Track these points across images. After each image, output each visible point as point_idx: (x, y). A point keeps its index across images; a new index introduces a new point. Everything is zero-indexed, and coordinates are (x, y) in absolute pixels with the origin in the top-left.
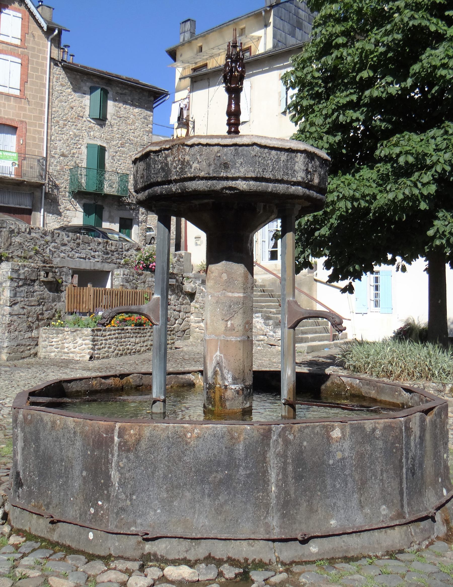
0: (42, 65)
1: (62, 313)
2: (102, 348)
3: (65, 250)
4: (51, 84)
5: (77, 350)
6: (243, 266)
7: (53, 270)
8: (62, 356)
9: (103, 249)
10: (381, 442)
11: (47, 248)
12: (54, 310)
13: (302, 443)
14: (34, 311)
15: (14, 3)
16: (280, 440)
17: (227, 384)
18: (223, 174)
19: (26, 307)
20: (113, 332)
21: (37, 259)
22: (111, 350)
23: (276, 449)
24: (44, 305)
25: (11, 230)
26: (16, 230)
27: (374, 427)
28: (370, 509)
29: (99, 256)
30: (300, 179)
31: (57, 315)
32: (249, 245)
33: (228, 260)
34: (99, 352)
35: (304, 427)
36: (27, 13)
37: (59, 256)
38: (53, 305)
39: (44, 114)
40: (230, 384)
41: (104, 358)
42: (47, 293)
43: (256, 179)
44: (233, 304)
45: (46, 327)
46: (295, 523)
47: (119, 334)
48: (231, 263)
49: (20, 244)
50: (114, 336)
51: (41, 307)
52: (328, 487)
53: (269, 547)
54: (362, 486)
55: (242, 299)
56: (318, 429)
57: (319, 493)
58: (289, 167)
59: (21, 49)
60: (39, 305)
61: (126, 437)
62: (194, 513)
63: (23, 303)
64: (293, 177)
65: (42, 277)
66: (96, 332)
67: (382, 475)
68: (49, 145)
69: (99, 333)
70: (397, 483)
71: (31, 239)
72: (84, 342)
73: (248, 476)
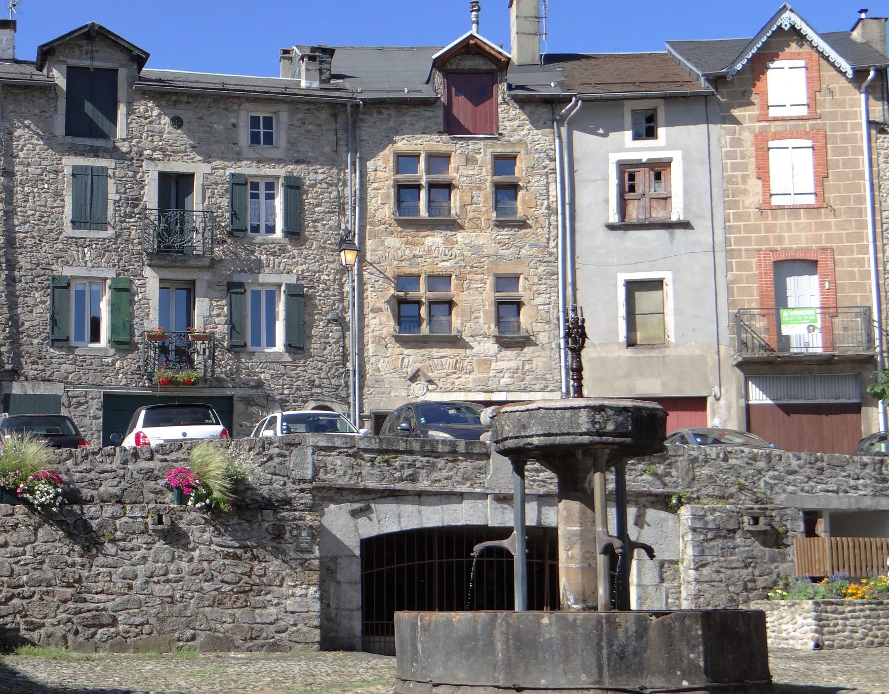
0: (854, 139)
1: (790, 580)
2: (839, 631)
3: (794, 480)
4: (875, 169)
5: (797, 634)
7: (768, 513)
8: (779, 644)
9: (873, 474)
11: (759, 479)
12: (774, 576)
14: (737, 576)
15: (789, 46)
18: (523, 434)
19: (722, 570)
20: (858, 608)
21: (743, 497)
22: (856, 635)
24: (755, 567)
25: (691, 457)
26: (701, 458)
29: (866, 486)
30: (584, 430)
31: (781, 583)
32: (586, 485)
33: (567, 498)
34: (831, 637)
36: (816, 55)
37: (784, 491)
38: (772, 567)
39: (866, 227)
41: (843, 647)
42: (758, 548)
43: (545, 435)
45: (759, 601)
47: (872, 610)
49: (710, 477)
50: (862, 614)
51: (750, 570)
54: (567, 658)
56: (531, 617)
58: (573, 422)
59: (811, 122)
60: (746, 567)
63: (716, 564)
65: (746, 525)
66: (822, 606)
68: (881, 282)
69: (829, 608)
71: (730, 469)
72: (805, 622)
73: (484, 646)
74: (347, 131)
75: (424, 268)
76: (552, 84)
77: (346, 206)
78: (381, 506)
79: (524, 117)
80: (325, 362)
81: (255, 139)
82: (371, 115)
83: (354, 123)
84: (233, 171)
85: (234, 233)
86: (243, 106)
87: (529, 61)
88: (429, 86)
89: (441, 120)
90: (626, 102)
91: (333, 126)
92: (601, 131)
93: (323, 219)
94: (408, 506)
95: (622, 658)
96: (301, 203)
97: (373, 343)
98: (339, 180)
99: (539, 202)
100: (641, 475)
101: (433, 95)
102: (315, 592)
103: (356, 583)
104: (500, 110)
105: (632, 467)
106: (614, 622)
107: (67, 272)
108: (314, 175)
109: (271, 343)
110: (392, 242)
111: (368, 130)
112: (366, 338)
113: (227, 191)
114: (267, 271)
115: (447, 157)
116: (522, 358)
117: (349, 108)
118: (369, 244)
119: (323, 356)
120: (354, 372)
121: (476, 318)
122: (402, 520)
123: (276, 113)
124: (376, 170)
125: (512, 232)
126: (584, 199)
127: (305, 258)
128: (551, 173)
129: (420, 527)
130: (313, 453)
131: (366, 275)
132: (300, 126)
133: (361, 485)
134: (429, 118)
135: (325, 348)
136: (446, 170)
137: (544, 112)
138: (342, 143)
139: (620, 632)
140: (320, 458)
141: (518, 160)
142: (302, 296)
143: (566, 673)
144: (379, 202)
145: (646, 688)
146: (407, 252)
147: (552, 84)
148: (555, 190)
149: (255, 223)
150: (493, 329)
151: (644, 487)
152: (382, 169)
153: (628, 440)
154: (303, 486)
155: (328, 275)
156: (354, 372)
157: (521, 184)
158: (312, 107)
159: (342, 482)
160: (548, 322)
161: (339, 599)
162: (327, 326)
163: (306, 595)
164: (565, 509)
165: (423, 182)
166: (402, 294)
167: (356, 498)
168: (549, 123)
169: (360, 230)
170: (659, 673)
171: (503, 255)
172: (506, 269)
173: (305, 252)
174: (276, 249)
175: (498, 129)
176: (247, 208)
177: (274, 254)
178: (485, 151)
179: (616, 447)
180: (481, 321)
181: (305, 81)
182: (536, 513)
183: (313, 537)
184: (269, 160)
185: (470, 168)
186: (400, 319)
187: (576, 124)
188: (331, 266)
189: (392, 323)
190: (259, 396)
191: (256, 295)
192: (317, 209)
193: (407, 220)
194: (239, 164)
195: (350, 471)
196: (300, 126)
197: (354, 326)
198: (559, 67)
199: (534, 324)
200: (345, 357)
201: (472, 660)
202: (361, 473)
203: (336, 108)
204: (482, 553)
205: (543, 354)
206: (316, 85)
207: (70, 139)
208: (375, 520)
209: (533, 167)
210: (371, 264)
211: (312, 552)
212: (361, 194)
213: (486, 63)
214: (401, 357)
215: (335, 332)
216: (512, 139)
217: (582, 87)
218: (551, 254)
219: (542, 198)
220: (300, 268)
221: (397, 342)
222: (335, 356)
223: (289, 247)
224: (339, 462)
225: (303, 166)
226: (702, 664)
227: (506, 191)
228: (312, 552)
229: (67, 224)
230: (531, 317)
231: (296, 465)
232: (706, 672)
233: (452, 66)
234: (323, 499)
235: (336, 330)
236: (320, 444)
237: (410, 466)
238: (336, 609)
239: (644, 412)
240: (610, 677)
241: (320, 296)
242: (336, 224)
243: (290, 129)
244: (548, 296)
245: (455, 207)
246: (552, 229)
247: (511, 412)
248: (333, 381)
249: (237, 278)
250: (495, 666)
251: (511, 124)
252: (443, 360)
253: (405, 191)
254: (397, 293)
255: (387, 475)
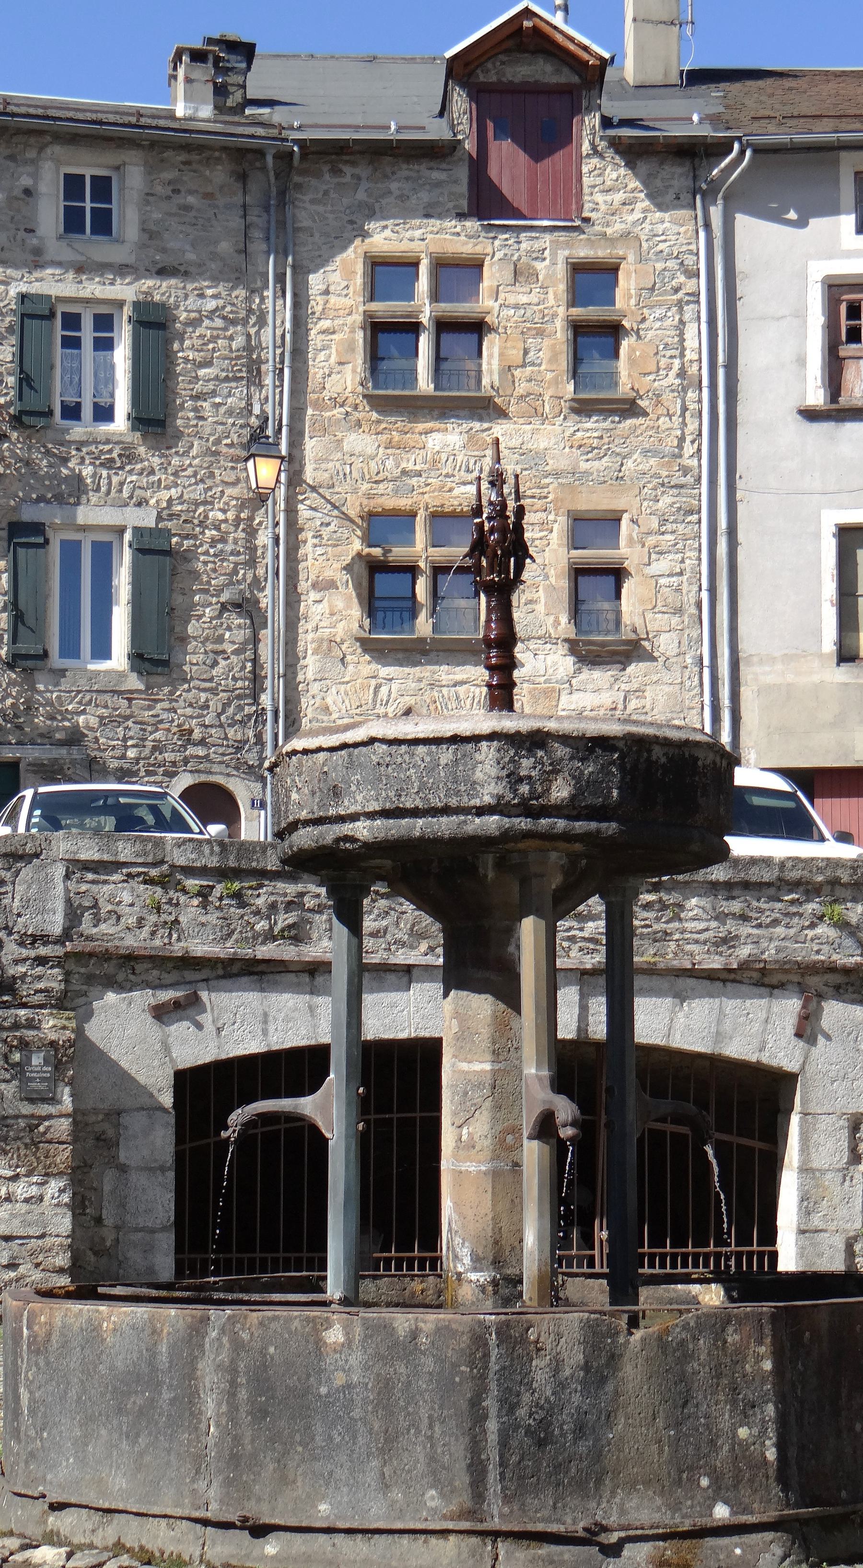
6: (490, 998)
10: (431, 1359)
13: (266, 1349)
16: (225, 1340)
17: (460, 1269)
18: (332, 812)
23: (218, 1355)
27: (413, 1327)
28: (405, 1494)
30: (487, 799)
33: (460, 987)
35: (268, 1318)
40: (467, 1271)
43: (385, 814)
44: (472, 1089)
46: (249, 1499)
48: (465, 993)
52: (317, 1438)
53: (195, 1533)
54: (389, 1444)
55: (489, 1076)
57: (300, 1449)
58: (459, 777)
61: (36, 1328)
62: (111, 1467)
64: (471, 797)
67: (431, 1427)
70: (463, 1447)
73: (173, 1401)
74: (267, 209)
76: (695, 118)
77: (264, 368)
78: (224, 995)
79: (634, 184)
80: (214, 691)
81: (73, 222)
82: (318, 175)
83: (282, 193)
84: (24, 288)
85: (25, 419)
86: (49, 151)
87: (658, 79)
88: (443, 122)
89: (463, 188)
90: (843, 154)
91: (238, 199)
92: (792, 215)
93: (214, 393)
94: (286, 996)
95: (541, 1443)
96: (169, 358)
97: (316, 652)
98: (250, 311)
99: (663, 362)
100: (813, 926)
101: (447, 135)
102: (62, 1191)
103: (163, 1169)
104: (585, 169)
105: (793, 909)
106: (523, 1340)
108: (194, 301)
109: (102, 650)
110: (359, 442)
111: (309, 209)
112: (301, 644)
113: (10, 329)
114: (94, 500)
115: (474, 267)
116: (623, 687)
117: (270, 159)
118: (311, 446)
119: (211, 680)
120: (276, 713)
121: (530, 602)
122: (271, 1028)
123: (117, 168)
124: (327, 292)
125: (607, 424)
126: (754, 356)
127: (176, 474)
128: (688, 303)
129: (313, 1042)
130: (67, 877)
131: (303, 512)
132: (169, 198)
133: (178, 949)
134: (438, 184)
135: (215, 663)
136: (474, 293)
137: (676, 175)
138: (257, 234)
139: (540, 1369)
140: (84, 887)
141: (621, 274)
142: (168, 552)
143: (385, 1486)
144: (333, 359)
145: (605, 1529)
146: (390, 463)
147: (695, 118)
148: (695, 338)
149: (71, 399)
150: (564, 626)
151: (818, 952)
152: (339, 291)
153: (611, 828)
154: (43, 951)
155: (224, 511)
156: (276, 713)
157: (626, 323)
158: (195, 157)
159: (132, 942)
160: (679, 611)
161: (123, 1205)
162: (220, 616)
163: (41, 1199)
164: (456, 1015)
165: (425, 319)
166: (377, 551)
167: (168, 978)
168: (686, 197)
169: (291, 417)
170: (647, 1483)
171: (586, 472)
173: (175, 461)
174: (115, 455)
175: (581, 208)
176: (52, 367)
177: (109, 464)
178: (554, 255)
179: (578, 847)
180: (540, 608)
181: (187, 104)
182: (576, 1010)
183: (58, 1066)
184: (100, 268)
185: (522, 290)
186: (372, 604)
187: (738, 200)
188: (229, 491)
189: (356, 612)
190: (73, 762)
191: (71, 550)
192: (202, 372)
193: (389, 397)
194: (37, 274)
195: (153, 918)
196: (169, 198)
197: (277, 617)
198: (715, 92)
199: (649, 616)
200: (256, 680)
201: (142, 1441)
202: (176, 921)
203: (243, 158)
204: (248, 1125)
205: (667, 677)
206: (206, 111)
208: (209, 1027)
209: (653, 289)
210: (314, 489)
211: (53, 1100)
212: (294, 341)
213: (558, 71)
214: (373, 682)
215: (236, 631)
216: (609, 231)
217: (756, 124)
218: (685, 471)
219: (669, 353)
220: (165, 495)
221: (366, 651)
222: (235, 679)
223: (142, 450)
224: (126, 897)
225: (173, 281)
226: (771, 1454)
227: (596, 338)
228: (53, 1100)
230: (642, 601)
231: (26, 903)
232: (783, 1478)
233: (489, 76)
234: (90, 979)
235: (239, 626)
236: (83, 857)
237: (290, 906)
238: (118, 1228)
239: (657, 752)
240: (507, 1499)
241: (207, 553)
242: (243, 404)
243: (148, 203)
244: (680, 556)
245: (491, 372)
246: (688, 419)
247: (305, 752)
248: (231, 733)
249: (28, 514)
250: (198, 1462)
251: (609, 198)
252: (461, 690)
253: (387, 337)
254: (367, 550)
255: (237, 925)
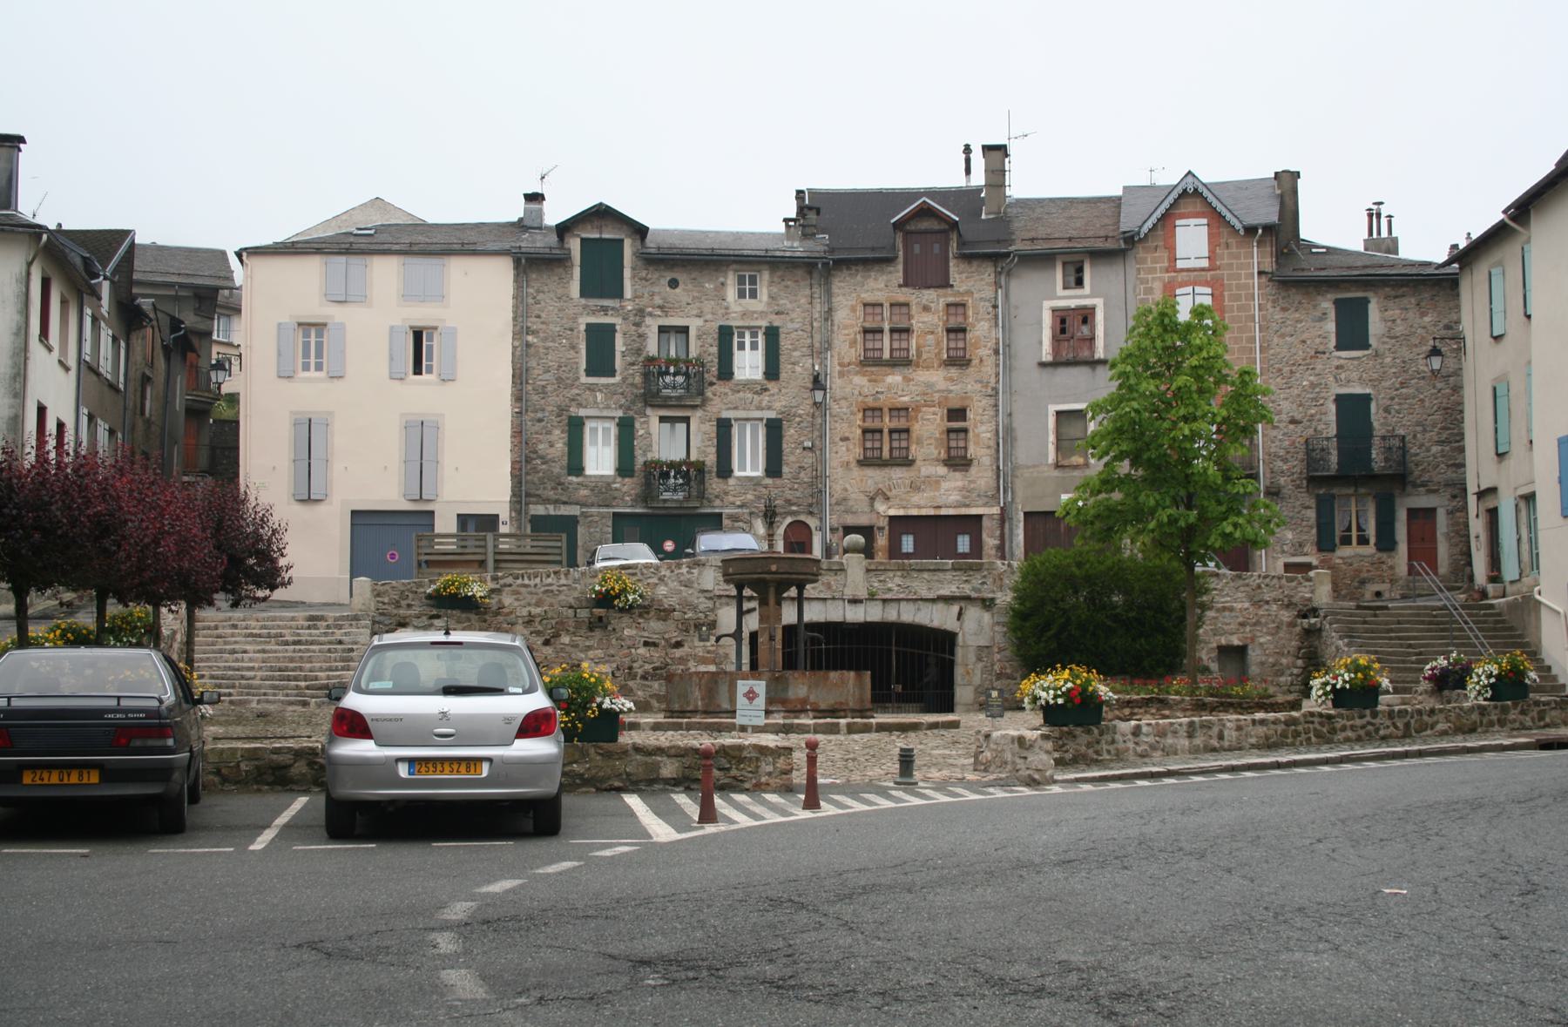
75: (884, 401)
107: (582, 412)
172: (956, 404)
207: (583, 301)
229: (582, 372)
